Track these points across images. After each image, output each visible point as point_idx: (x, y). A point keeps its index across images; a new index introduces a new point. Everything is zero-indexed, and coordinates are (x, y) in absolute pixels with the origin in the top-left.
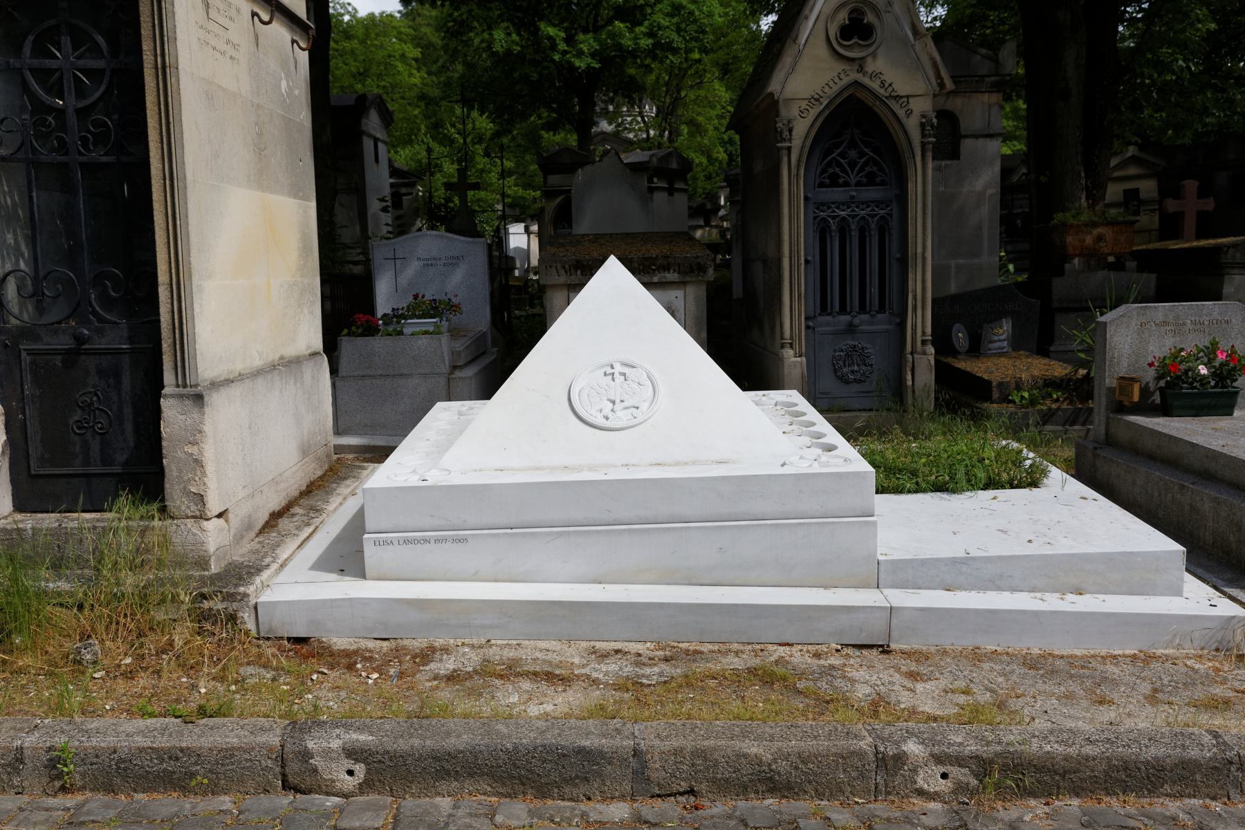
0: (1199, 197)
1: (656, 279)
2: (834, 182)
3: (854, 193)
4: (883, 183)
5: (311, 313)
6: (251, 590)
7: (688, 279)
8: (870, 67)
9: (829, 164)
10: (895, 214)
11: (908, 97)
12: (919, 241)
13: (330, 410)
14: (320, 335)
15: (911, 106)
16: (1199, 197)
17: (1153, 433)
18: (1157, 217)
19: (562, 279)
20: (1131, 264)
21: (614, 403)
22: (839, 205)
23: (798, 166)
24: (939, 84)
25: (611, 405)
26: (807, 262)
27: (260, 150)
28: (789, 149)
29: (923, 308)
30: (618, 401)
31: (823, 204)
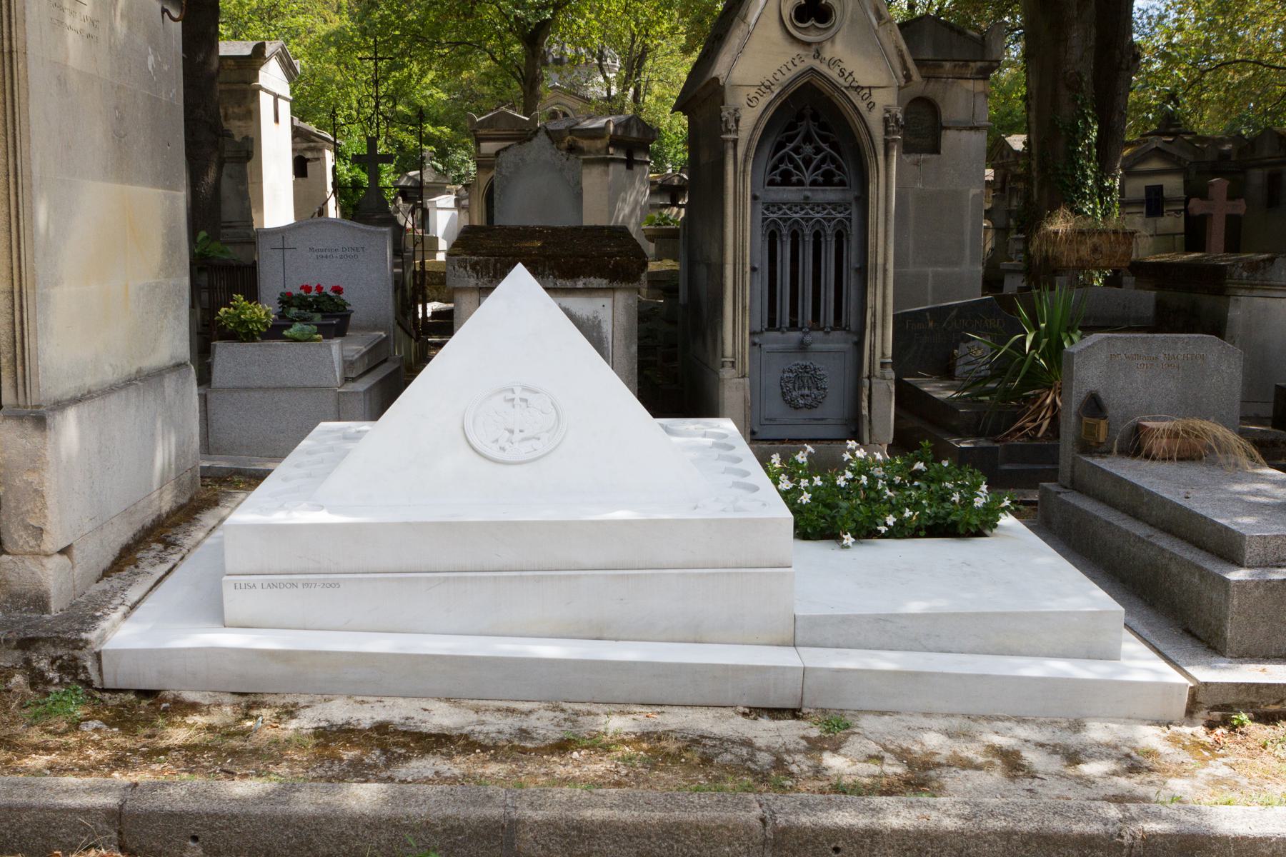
0: (1230, 198)
1: (580, 284)
2: (786, 180)
3: (809, 194)
4: (842, 183)
5: (177, 318)
6: (92, 636)
7: (615, 285)
8: (828, 53)
9: (781, 160)
10: (854, 217)
11: (870, 88)
12: (881, 250)
13: (196, 428)
14: (187, 343)
15: (873, 99)
16: (1230, 198)
17: (1119, 481)
18: (1182, 219)
19: (472, 282)
20: (1129, 280)
21: (512, 432)
22: (792, 206)
23: (745, 161)
24: (905, 76)
25: (507, 434)
26: (753, 269)
27: (119, 136)
28: (735, 142)
29: (884, 327)
30: (517, 431)
31: (773, 205)
